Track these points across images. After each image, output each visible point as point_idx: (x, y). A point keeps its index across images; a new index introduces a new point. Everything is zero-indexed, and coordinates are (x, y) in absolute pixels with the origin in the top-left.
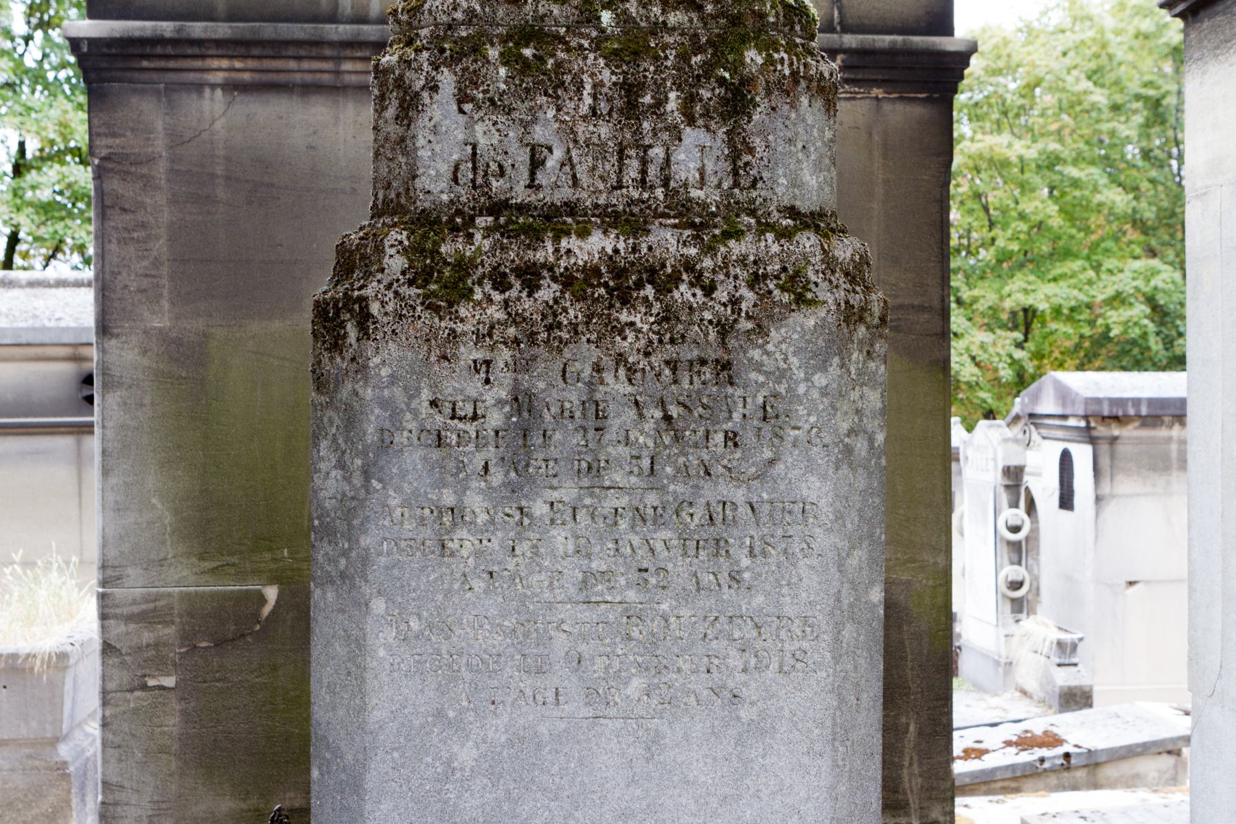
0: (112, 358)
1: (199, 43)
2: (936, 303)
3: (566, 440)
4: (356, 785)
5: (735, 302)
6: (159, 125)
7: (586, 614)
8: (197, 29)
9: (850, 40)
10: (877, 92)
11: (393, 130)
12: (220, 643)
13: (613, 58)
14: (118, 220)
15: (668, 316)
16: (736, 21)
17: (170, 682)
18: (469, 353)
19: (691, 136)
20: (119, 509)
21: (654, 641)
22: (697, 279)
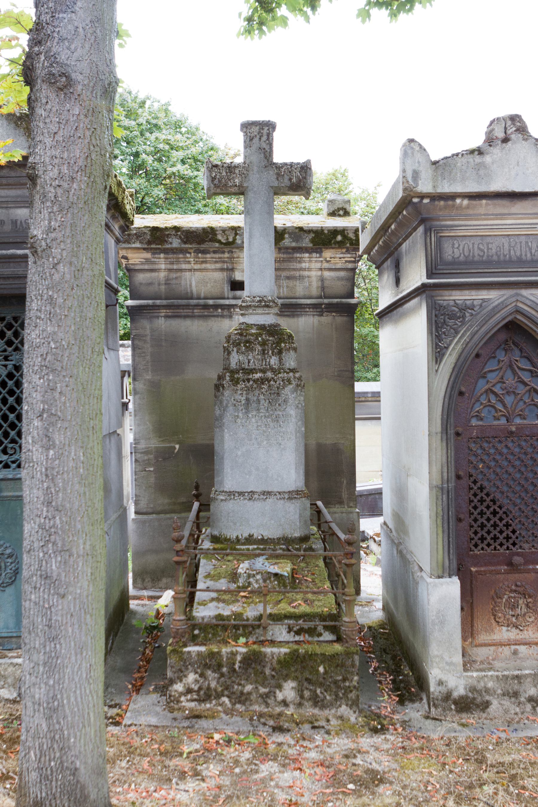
0: (137, 386)
1: (158, 306)
2: (350, 369)
3: (254, 405)
4: (223, 458)
5: (280, 384)
6: (148, 327)
7: (258, 432)
8: (158, 302)
9: (326, 301)
10: (333, 314)
11: (227, 357)
12: (164, 459)
13: (261, 345)
14: (138, 351)
15: (269, 386)
16: (280, 339)
17: (152, 469)
18: (239, 392)
19: (273, 358)
20: (139, 425)
21: (268, 436)
22: (274, 381)
